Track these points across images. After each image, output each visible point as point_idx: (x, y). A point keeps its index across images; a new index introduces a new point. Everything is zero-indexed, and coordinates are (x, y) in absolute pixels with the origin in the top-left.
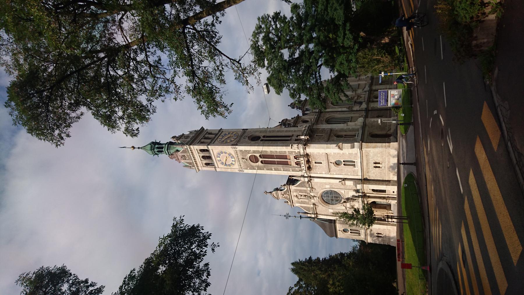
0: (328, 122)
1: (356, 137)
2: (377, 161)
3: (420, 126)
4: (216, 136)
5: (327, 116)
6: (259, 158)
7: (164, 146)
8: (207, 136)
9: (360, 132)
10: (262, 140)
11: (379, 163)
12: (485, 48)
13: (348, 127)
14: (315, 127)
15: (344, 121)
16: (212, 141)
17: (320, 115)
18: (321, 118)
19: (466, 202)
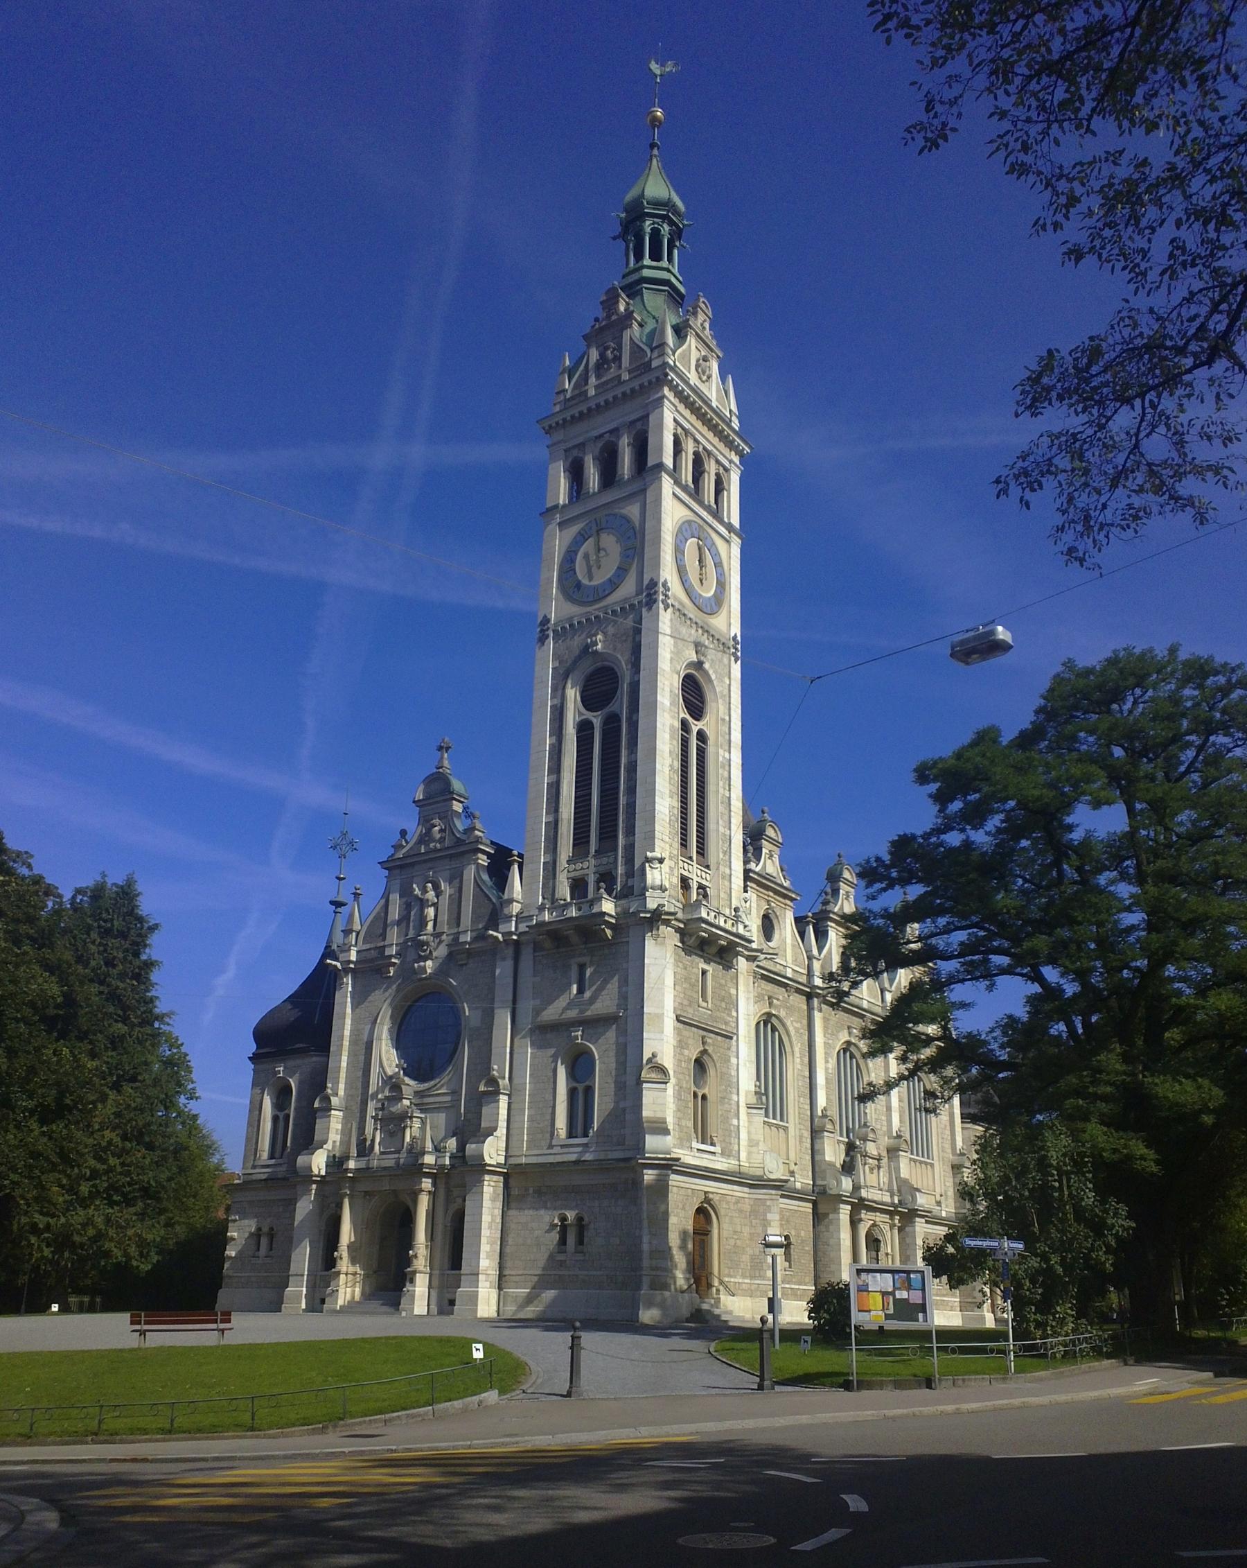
0: (767, 1023)
1: (695, 1145)
2: (588, 1234)
3: (787, 1475)
4: (707, 508)
5: (794, 1026)
6: (607, 710)
7: (665, 263)
8: (711, 468)
9: (720, 1164)
10: (685, 726)
11: (580, 1241)
12: (995, 1176)
13: (743, 1110)
14: (742, 963)
15: (770, 1100)
16: (685, 488)
17: (798, 991)
18: (780, 993)
19: (128, 1518)
